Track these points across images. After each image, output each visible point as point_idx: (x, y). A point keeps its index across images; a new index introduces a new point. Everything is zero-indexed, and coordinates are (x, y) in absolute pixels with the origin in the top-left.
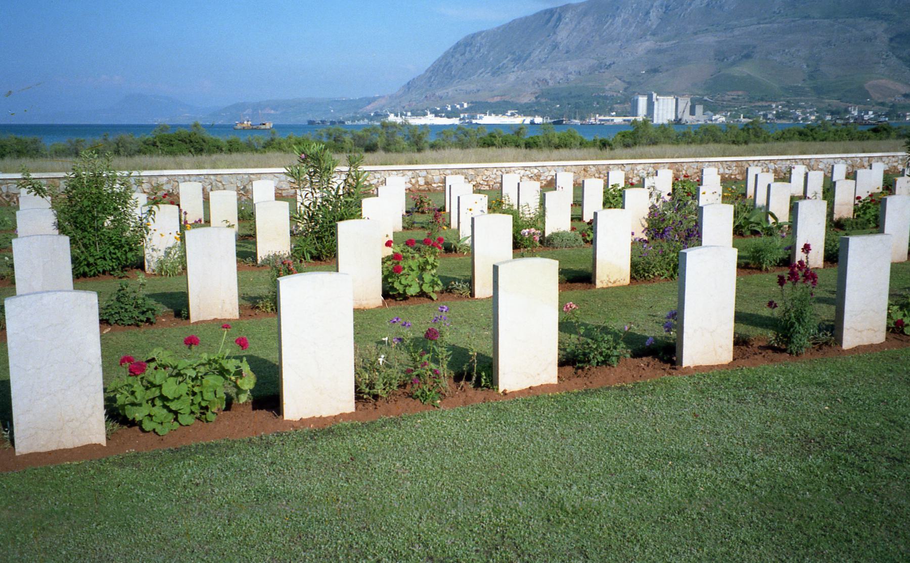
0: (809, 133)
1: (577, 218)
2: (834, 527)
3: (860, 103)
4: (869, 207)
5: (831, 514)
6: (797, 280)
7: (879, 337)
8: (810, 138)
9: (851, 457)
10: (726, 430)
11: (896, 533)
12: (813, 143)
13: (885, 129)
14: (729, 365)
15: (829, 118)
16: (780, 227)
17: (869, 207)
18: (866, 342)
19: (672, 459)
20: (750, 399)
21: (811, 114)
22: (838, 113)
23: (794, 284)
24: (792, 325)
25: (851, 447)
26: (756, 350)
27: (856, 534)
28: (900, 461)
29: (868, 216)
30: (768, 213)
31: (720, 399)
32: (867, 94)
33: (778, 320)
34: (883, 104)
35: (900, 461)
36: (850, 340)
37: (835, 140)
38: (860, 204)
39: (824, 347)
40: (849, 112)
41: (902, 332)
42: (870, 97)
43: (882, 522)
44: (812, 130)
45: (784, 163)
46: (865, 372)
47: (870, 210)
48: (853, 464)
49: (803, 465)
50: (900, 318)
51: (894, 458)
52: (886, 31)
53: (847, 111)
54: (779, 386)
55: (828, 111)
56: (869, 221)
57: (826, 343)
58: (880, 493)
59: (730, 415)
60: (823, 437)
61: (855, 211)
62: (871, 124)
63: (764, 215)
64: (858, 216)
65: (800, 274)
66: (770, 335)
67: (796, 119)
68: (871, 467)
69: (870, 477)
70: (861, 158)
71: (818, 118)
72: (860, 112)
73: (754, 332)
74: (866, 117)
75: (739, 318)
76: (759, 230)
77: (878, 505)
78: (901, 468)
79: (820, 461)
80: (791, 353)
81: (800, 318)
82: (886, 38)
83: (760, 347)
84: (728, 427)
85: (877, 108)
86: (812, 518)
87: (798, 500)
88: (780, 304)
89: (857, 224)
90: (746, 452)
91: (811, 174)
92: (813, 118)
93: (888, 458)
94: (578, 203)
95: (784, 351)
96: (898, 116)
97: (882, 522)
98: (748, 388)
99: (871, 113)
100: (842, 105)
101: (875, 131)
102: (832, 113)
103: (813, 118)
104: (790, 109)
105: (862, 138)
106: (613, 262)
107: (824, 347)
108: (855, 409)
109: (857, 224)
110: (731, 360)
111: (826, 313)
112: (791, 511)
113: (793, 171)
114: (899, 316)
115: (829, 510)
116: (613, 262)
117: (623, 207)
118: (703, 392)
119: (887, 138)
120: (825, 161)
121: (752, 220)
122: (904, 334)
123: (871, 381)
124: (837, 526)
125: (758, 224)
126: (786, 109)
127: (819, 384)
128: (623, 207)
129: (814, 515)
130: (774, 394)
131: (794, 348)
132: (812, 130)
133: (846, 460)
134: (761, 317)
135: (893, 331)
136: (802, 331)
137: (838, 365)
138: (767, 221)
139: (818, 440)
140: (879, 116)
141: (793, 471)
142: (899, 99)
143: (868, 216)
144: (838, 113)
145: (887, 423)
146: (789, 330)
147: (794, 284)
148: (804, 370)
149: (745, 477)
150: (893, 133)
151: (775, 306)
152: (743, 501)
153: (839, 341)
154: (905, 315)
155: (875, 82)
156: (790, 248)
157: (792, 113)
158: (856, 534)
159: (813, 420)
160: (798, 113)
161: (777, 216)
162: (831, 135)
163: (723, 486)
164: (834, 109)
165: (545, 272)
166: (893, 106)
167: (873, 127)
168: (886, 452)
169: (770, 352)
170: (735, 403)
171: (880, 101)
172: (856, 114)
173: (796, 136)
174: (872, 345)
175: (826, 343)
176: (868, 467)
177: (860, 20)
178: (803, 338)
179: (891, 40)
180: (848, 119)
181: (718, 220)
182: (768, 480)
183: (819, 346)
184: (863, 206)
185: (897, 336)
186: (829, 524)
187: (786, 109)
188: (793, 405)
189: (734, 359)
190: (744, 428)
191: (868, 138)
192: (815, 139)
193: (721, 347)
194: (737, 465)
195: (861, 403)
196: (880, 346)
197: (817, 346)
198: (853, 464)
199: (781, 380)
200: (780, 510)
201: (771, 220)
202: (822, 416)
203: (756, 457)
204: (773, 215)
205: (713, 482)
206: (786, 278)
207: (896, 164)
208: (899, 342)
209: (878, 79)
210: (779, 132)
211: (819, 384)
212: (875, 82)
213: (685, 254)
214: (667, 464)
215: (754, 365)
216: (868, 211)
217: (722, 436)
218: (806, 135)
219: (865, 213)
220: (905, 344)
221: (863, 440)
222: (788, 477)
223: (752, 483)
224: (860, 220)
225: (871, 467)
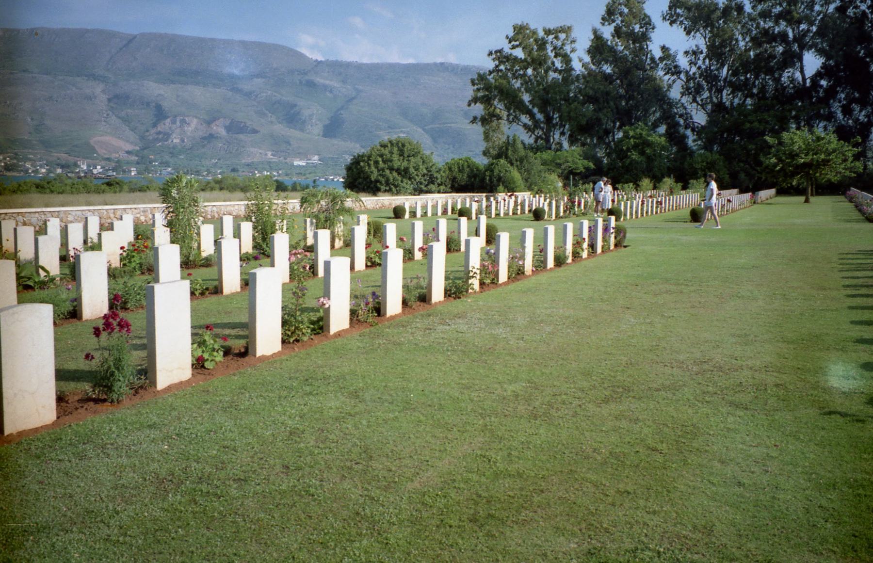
3: (88, 158)
4: (134, 257)
5: (207, 543)
6: (113, 329)
8: (48, 190)
9: (204, 487)
10: (78, 490)
12: (52, 196)
13: (118, 183)
14: (53, 424)
15: (59, 171)
16: (52, 280)
17: (134, 257)
19: (32, 534)
20: (91, 453)
21: (41, 166)
22: (68, 166)
23: (110, 334)
24: (112, 374)
25: (200, 479)
26: (76, 404)
27: (235, 555)
28: (245, 480)
29: (133, 265)
30: (38, 267)
31: (60, 460)
33: (96, 372)
34: (108, 159)
35: (245, 480)
36: (163, 380)
37: (72, 193)
38: (125, 254)
39: (140, 391)
40: (79, 166)
41: (203, 366)
43: (251, 538)
44: (48, 183)
45: (32, 215)
47: (135, 259)
48: (208, 492)
49: (166, 505)
50: (200, 354)
51: (239, 479)
52: (103, 91)
53: (76, 165)
55: (58, 165)
56: (134, 268)
57: (141, 387)
59: (77, 473)
60: (173, 474)
61: (121, 260)
63: (34, 269)
64: (124, 265)
65: (115, 323)
66: (87, 387)
67: (26, 171)
68: (225, 492)
69: (226, 501)
70: (107, 210)
71: (49, 171)
72: (89, 166)
73: (71, 386)
74: (95, 172)
75: (61, 375)
76: (32, 284)
77: (242, 524)
79: (179, 497)
80: (112, 402)
82: (104, 97)
83: (79, 401)
84: (79, 487)
85: (104, 163)
86: (192, 552)
87: (173, 539)
88: (97, 355)
90: (107, 507)
91: (20, 229)
92: (44, 171)
93: (234, 480)
95: (105, 400)
96: (124, 171)
97: (251, 538)
98: (84, 444)
99: (99, 167)
100: (71, 159)
101: (109, 184)
102: (62, 167)
103: (44, 171)
104: (19, 161)
105: (98, 191)
107: (140, 391)
108: (190, 442)
109: (125, 272)
111: (135, 358)
112: (171, 550)
113: (48, 224)
114: (199, 353)
115: (204, 540)
117: (273, 265)
118: (38, 457)
119: (120, 191)
120: (73, 213)
121: (23, 275)
122: (205, 368)
123: (194, 415)
125: (29, 279)
126: (15, 161)
128: (273, 265)
131: (115, 396)
132: (48, 183)
134: (69, 371)
135: (196, 368)
136: (121, 379)
137: (160, 405)
138: (38, 274)
139: (170, 478)
140: (107, 170)
141: (158, 513)
142: (123, 156)
143: (133, 265)
144: (68, 166)
145: (222, 449)
146: (109, 379)
147: (110, 334)
148: (131, 415)
151: (93, 358)
152: (122, 555)
153: (153, 383)
154: (203, 352)
155: (100, 138)
156: (75, 300)
158: (235, 555)
159: (159, 461)
160: (28, 165)
161: (48, 269)
162: (68, 188)
163: (98, 546)
164: (64, 162)
167: (107, 181)
168: (231, 475)
169: (91, 404)
173: (34, 189)
174: (181, 383)
175: (141, 387)
176: (221, 492)
177: (78, 79)
178: (121, 386)
179: (109, 100)
180: (78, 172)
182: (138, 527)
183: (137, 390)
184: (128, 255)
187: (15, 161)
188: (135, 451)
189: (58, 418)
190: (96, 484)
191: (104, 192)
192: (52, 192)
194: (102, 521)
195: (194, 436)
196: (188, 382)
197: (132, 391)
198: (208, 492)
199: (114, 429)
200: (160, 553)
202: (165, 456)
203: (119, 509)
204: (43, 269)
205: (85, 545)
206: (101, 329)
207: (138, 215)
208: (202, 376)
209: (101, 136)
211: (150, 427)
212: (100, 138)
213: (153, 287)
214: (27, 540)
215: (80, 420)
216: (133, 260)
217: (76, 498)
218: (43, 187)
220: (208, 377)
221: (208, 469)
222: (155, 520)
223: (125, 535)
224: (126, 269)
225: (225, 492)
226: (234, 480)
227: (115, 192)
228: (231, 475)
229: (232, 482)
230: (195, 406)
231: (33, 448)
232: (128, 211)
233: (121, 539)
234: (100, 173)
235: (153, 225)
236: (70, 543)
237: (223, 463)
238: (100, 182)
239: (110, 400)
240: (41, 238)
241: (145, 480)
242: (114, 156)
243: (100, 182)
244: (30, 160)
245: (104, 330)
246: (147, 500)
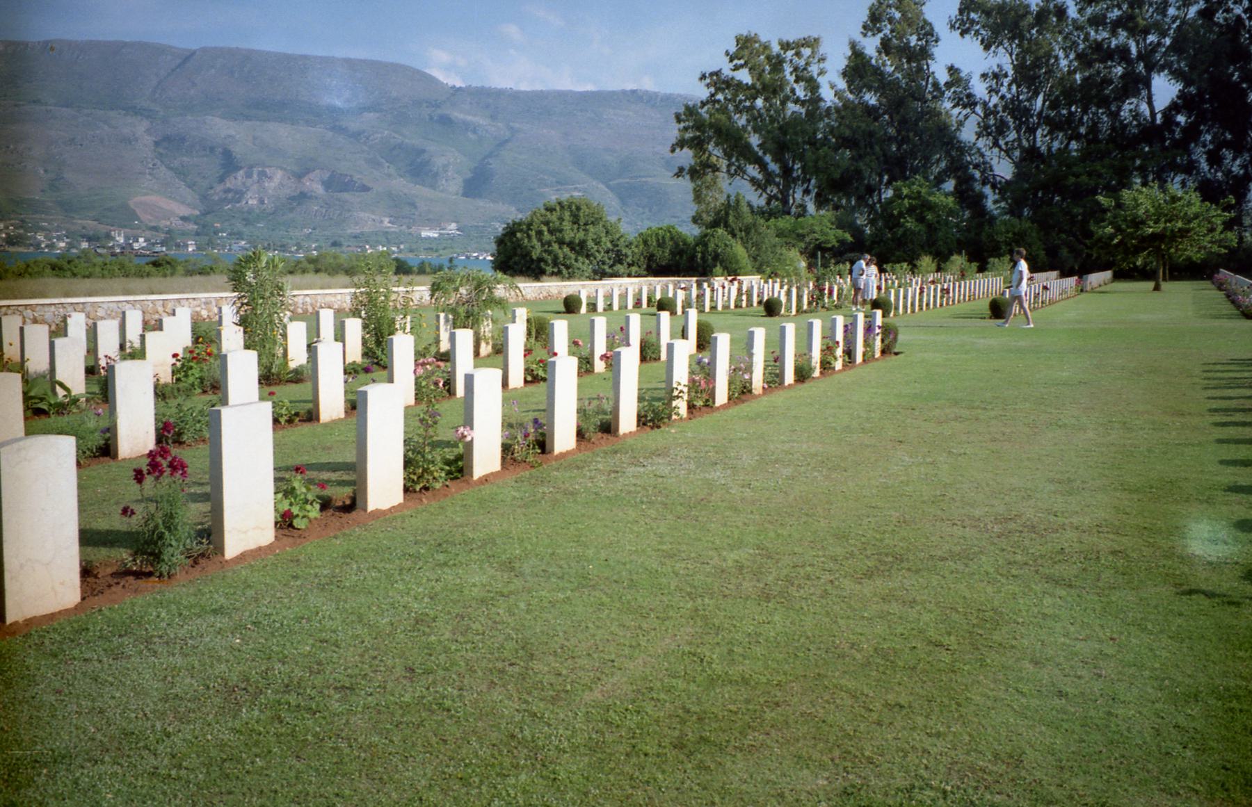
0: (66, 266)
1: (91, 371)
2: (308, 794)
3: (125, 227)
4: (191, 368)
5: (297, 778)
6: (162, 472)
7: (267, 536)
8: (69, 273)
9: (292, 699)
11: (381, 779)
12: (75, 281)
13: (168, 263)
14: (76, 608)
15: (85, 245)
16: (75, 401)
17: (191, 368)
18: (252, 546)
19: (45, 765)
20: (130, 650)
21: (59, 239)
23: (157, 478)
24: (161, 537)
25: (287, 686)
27: (337, 795)
28: (351, 689)
29: (191, 379)
31: (85, 660)
32: (134, 216)
33: (138, 533)
34: (155, 229)
35: (351, 689)
37: (103, 277)
38: (179, 364)
39: (201, 561)
40: (113, 239)
41: (291, 525)
42: (138, 219)
43: (360, 771)
44: (69, 262)
46: (266, 585)
47: (193, 371)
48: (298, 706)
50: (286, 507)
51: (343, 687)
52: (148, 131)
53: (109, 237)
54: (163, 625)
55: (83, 236)
56: (193, 385)
57: (203, 555)
58: (343, 735)
59: (110, 679)
60: (248, 680)
61: (173, 373)
62: (144, 256)
64: (178, 380)
65: (165, 464)
66: (124, 555)
67: (38, 246)
68: (322, 705)
69: (324, 718)
70: (153, 301)
71: (70, 246)
72: (127, 238)
74: (136, 246)
75: (88, 538)
76: (45, 407)
78: (354, 698)
79: (256, 713)
80: (161, 576)
81: (169, 520)
82: (149, 140)
84: (114, 698)
85: (148, 234)
86: (276, 792)
89: (179, 390)
90: (153, 726)
91: (29, 329)
92: (62, 245)
93: (336, 688)
94: (92, 350)
95: (150, 574)
96: (178, 246)
97: (360, 771)
98: (120, 636)
99: (141, 240)
100: (102, 229)
101: (156, 264)
102: (89, 239)
103: (62, 245)
104: (26, 231)
105: (141, 274)
106: (136, 429)
107: (201, 561)
109: (179, 390)
110: (78, 599)
111: (193, 513)
112: (245, 789)
113: (69, 321)
114: (285, 506)
115: (292, 774)
116: (136, 429)
118: (55, 656)
119: (172, 274)
120: (105, 306)
122: (293, 527)
123: (278, 595)
124: (311, 792)
125: (42, 399)
126: (21, 231)
127: (215, 612)
129: (276, 787)
130: (161, 637)
131: (165, 569)
132: (69, 262)
133: (289, 704)
134: (99, 533)
135: (281, 528)
136: (174, 543)
137: (229, 581)
138: (55, 394)
139: (243, 686)
140: (154, 244)
141: (227, 736)
142: (176, 223)
143: (191, 379)
144: (97, 239)
145: (318, 644)
147: (157, 478)
149: (166, 761)
150: (179, 268)
151: (133, 513)
152: (175, 796)
153: (220, 549)
154: (291, 504)
156: (108, 430)
157: (30, 238)
158: (337, 795)
159: (228, 661)
160: (40, 237)
161: (68, 385)
162: (98, 269)
163: (140, 783)
164: (91, 233)
165: (59, 453)
166: (169, 232)
168: (331, 681)
169: (131, 579)
170: (111, 661)
171: (153, 224)
172: (121, 240)
173: (48, 270)
174: (260, 549)
175: (203, 555)
176: (318, 706)
177: (112, 114)
178: (174, 553)
179: (157, 144)
180: (112, 247)
181: (242, 369)
182: (198, 756)
183: (196, 560)
184: (183, 365)
185: (286, 532)
186: (301, 792)
187: (21, 231)
188: (194, 647)
189: (83, 599)
190: (137, 694)
191: (148, 275)
192: (74, 275)
193: (62, 584)
194: (146, 747)
196: (270, 547)
197: (190, 561)
198: (298, 706)
199: (163, 615)
200: (230, 793)
201: (61, 392)
202: (237, 653)
203: (170, 729)
204: (62, 385)
206: (145, 472)
207: (198, 309)
208: (290, 540)
209: (146, 194)
210: (22, 265)
211: (215, 612)
213: (366, 393)
214: (39, 775)
215: (115, 601)
216: (190, 372)
218: (61, 269)
219: (186, 376)
220: (298, 541)
221: (298, 673)
222: (222, 746)
223: (180, 767)
224: (181, 385)
225: (322, 705)
226: (336, 688)
227: (165, 276)
228: (331, 681)
229: (332, 692)
230: (280, 582)
231: (47, 642)
232: (183, 302)
233: (173, 773)
234: (143, 248)
235: (220, 322)
236: (100, 779)
237: (320, 663)
238: (143, 261)
239: (157, 574)
240: (59, 342)
241: (208, 688)
242: (163, 223)
243: (143, 261)
244: (43, 229)
245: (149, 473)
246: (211, 716)
